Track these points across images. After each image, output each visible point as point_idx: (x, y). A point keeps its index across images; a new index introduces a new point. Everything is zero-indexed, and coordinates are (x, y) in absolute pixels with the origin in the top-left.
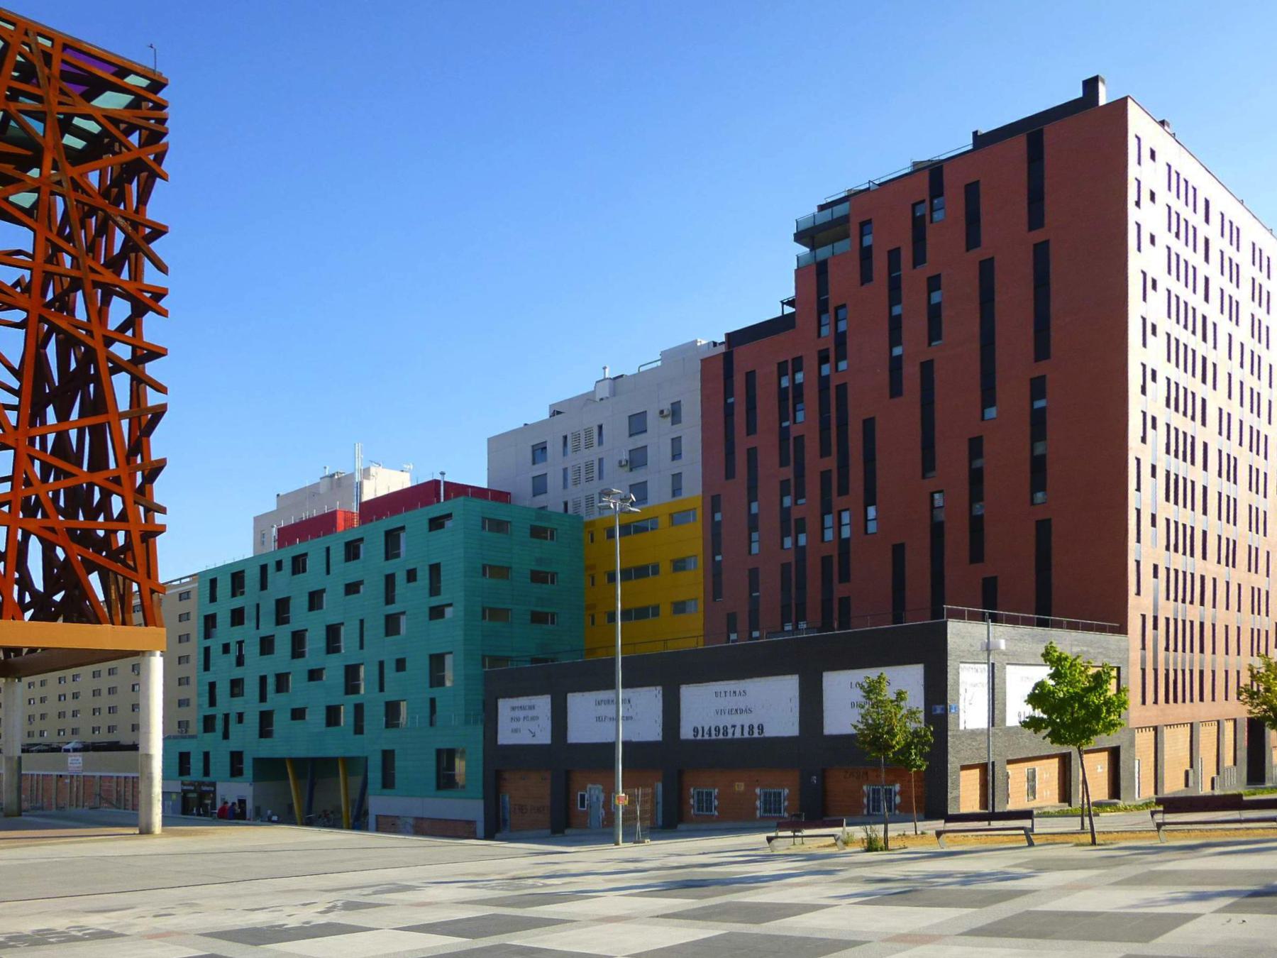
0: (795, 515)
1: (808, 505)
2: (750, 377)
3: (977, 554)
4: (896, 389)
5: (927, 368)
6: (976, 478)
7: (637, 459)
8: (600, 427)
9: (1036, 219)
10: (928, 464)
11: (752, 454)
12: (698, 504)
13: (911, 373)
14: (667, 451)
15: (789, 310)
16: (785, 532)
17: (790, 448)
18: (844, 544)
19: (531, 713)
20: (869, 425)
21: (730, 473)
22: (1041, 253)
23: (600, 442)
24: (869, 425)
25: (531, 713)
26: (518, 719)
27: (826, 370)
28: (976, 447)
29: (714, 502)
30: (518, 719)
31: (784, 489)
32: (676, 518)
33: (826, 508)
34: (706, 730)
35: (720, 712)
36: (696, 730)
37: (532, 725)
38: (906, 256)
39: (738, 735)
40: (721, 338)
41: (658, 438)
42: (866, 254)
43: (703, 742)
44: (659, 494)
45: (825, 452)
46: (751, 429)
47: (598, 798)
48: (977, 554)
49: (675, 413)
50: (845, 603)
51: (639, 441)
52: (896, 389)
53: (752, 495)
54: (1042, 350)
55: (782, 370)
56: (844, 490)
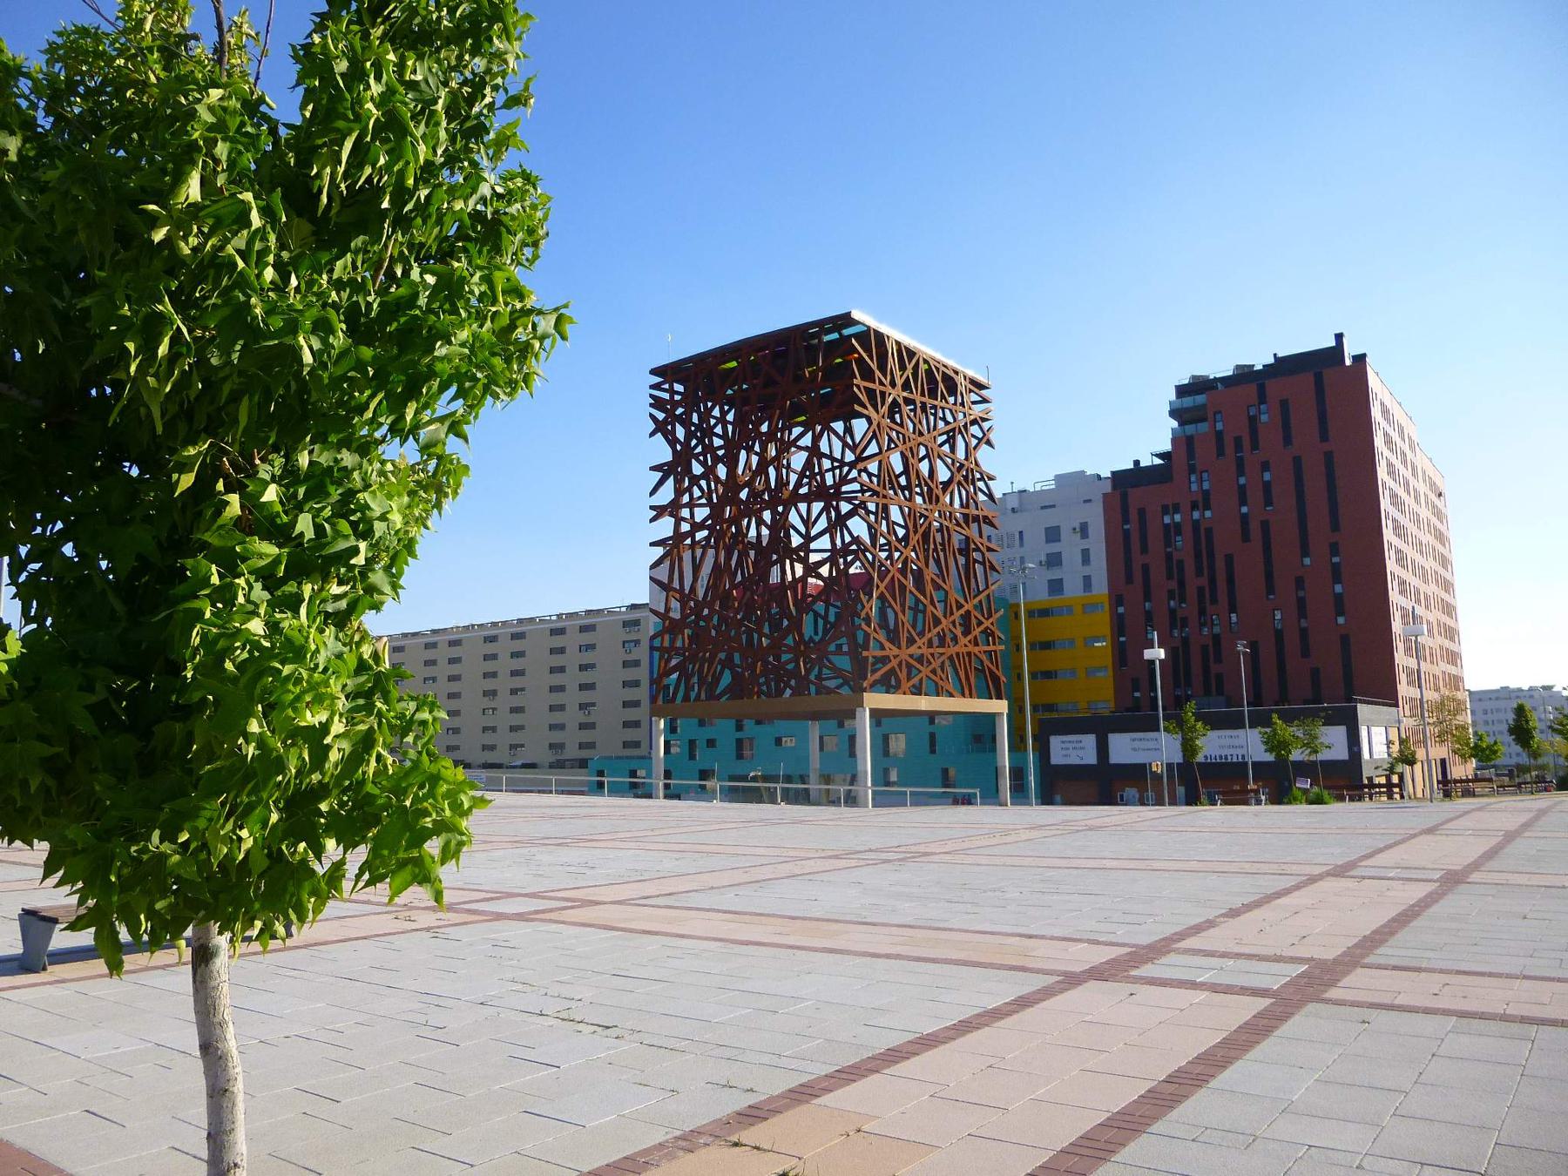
0: (1179, 614)
1: (1189, 609)
2: (1142, 512)
3: (1305, 653)
4: (1246, 537)
5: (1265, 526)
6: (1301, 604)
7: (1054, 560)
8: (1021, 533)
9: (1324, 437)
10: (1270, 589)
11: (1146, 569)
12: (1106, 600)
13: (1255, 527)
14: (1079, 558)
15: (1158, 461)
16: (1173, 626)
17: (1174, 568)
18: (1216, 639)
19: (1080, 745)
20: (1229, 559)
21: (1129, 579)
22: (1329, 456)
23: (1022, 544)
24: (1229, 559)
25: (1080, 745)
26: (1068, 749)
27: (1196, 515)
28: (1299, 583)
29: (1117, 599)
30: (1068, 749)
31: (1171, 595)
32: (1089, 608)
33: (1202, 612)
34: (1213, 756)
35: (1222, 747)
36: (1206, 757)
37: (1081, 753)
38: (1246, 443)
39: (1235, 760)
40: (1106, 473)
41: (1070, 547)
42: (1219, 436)
43: (1211, 764)
44: (1073, 589)
45: (1199, 572)
46: (1144, 549)
47: (1134, 797)
48: (1305, 653)
49: (1084, 530)
50: (1219, 677)
51: (1054, 548)
52: (1246, 537)
53: (1147, 596)
54: (1335, 526)
55: (1165, 510)
56: (1214, 601)
